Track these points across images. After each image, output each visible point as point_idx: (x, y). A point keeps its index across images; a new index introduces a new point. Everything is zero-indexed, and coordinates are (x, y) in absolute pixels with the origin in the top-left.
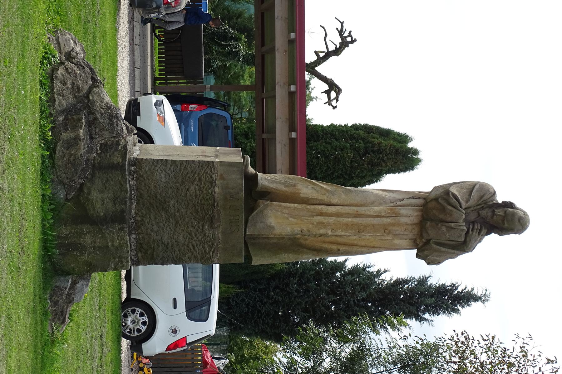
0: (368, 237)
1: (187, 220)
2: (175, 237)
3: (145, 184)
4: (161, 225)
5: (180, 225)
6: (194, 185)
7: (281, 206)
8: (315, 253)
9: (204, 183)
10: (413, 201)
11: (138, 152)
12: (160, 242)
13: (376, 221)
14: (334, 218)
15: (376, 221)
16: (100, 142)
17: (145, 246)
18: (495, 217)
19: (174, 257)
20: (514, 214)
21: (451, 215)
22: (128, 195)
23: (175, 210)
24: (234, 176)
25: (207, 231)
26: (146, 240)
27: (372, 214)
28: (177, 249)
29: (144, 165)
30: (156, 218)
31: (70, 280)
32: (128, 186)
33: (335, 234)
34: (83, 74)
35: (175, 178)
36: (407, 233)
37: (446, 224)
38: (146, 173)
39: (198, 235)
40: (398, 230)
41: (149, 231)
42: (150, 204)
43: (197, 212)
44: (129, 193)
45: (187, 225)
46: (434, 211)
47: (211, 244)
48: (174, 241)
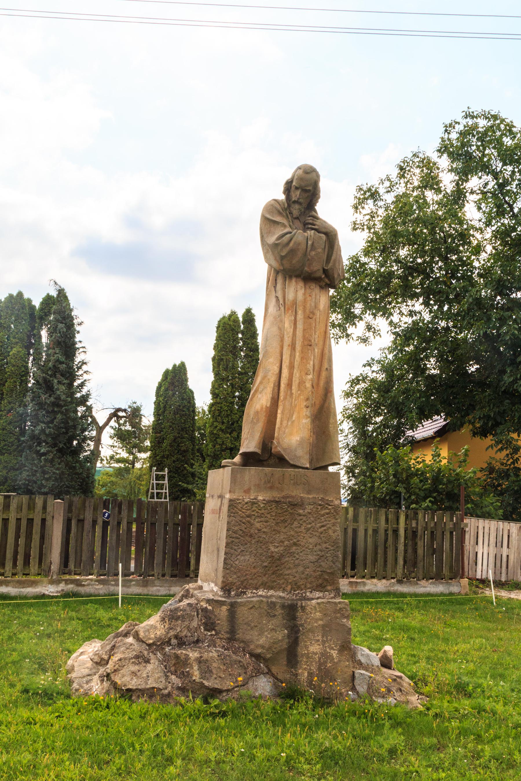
0: (317, 336)
1: (292, 533)
2: (311, 547)
3: (251, 579)
4: (297, 562)
5: (298, 541)
6: (255, 523)
7: (279, 428)
8: (329, 395)
9: (253, 511)
10: (279, 286)
11: (212, 585)
12: (316, 564)
13: (300, 326)
14: (295, 371)
15: (300, 326)
16: (202, 631)
17: (320, 581)
18: (301, 200)
19: (332, 548)
20: (300, 179)
21: (299, 244)
22: (264, 599)
23: (281, 546)
24: (247, 478)
25: (306, 511)
26: (313, 580)
27: (292, 330)
28: (324, 545)
29: (230, 579)
30: (289, 568)
31: (360, 671)
32: (254, 599)
33: (312, 371)
34: (122, 649)
35: (246, 544)
36: (314, 294)
37: (309, 249)
38: (238, 577)
39: (309, 521)
40: (310, 303)
41: (303, 576)
42: (273, 574)
43: (284, 521)
44: (261, 598)
45: (297, 533)
46: (294, 262)
47: (319, 507)
48: (315, 549)
